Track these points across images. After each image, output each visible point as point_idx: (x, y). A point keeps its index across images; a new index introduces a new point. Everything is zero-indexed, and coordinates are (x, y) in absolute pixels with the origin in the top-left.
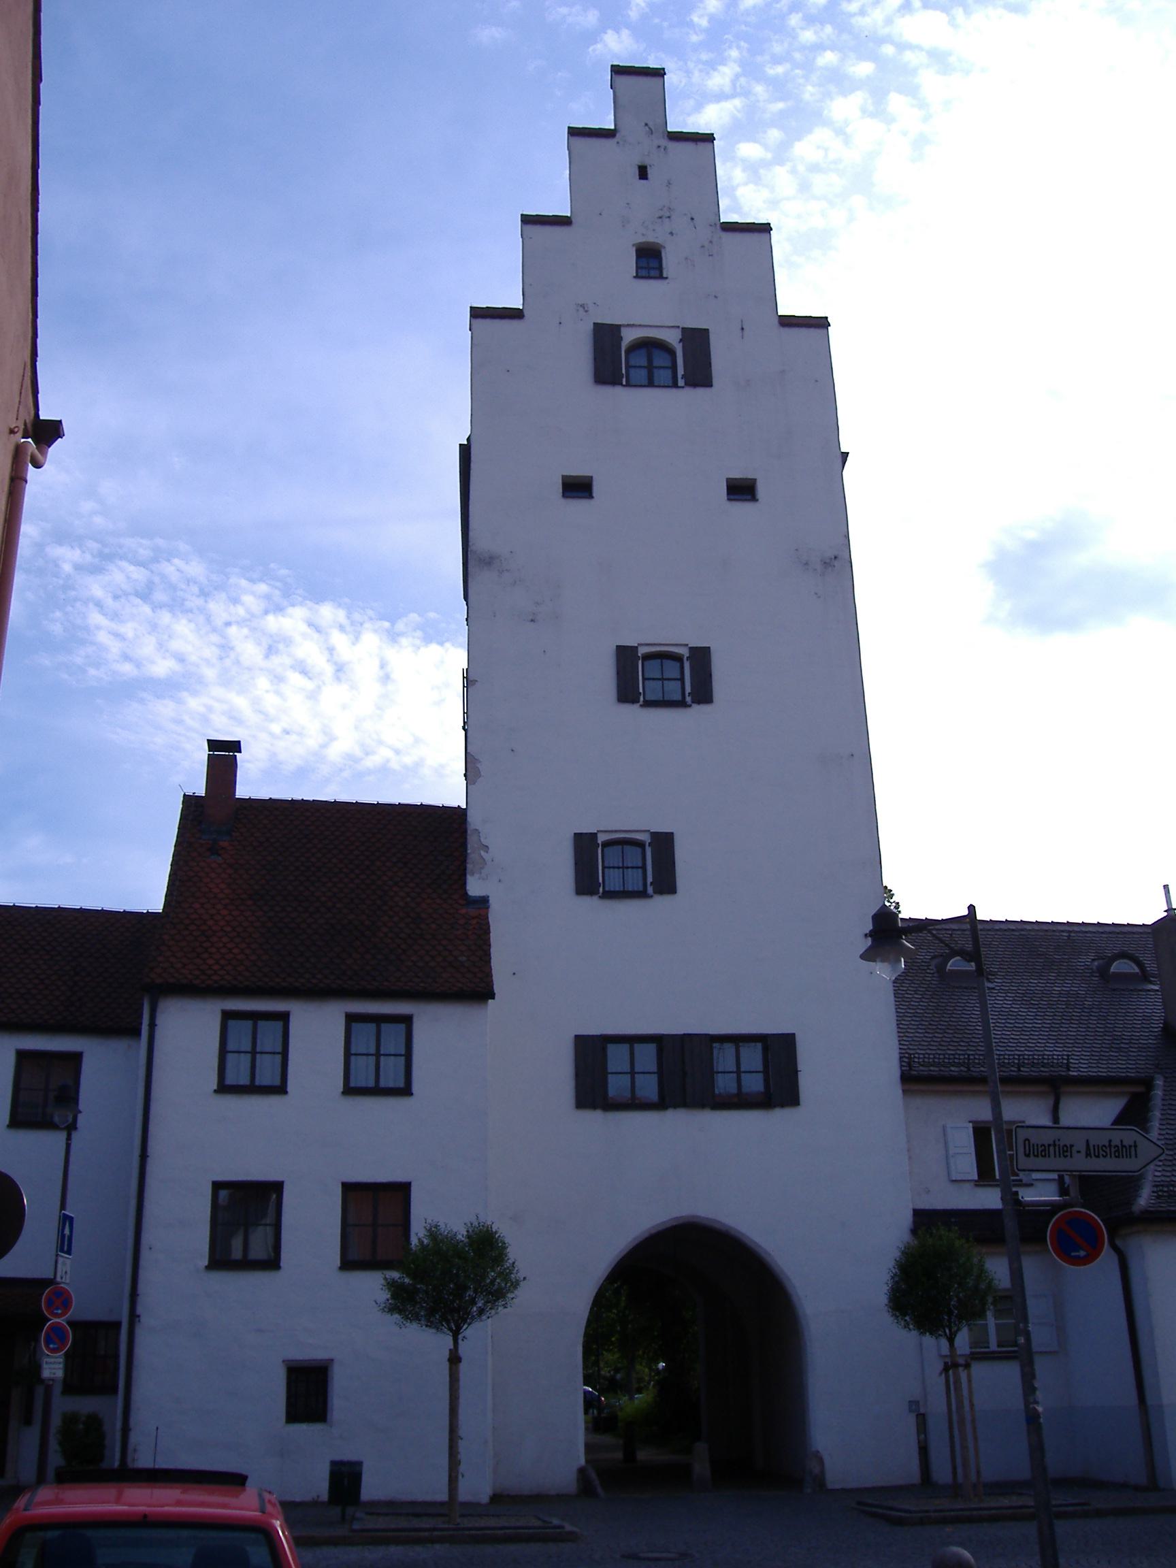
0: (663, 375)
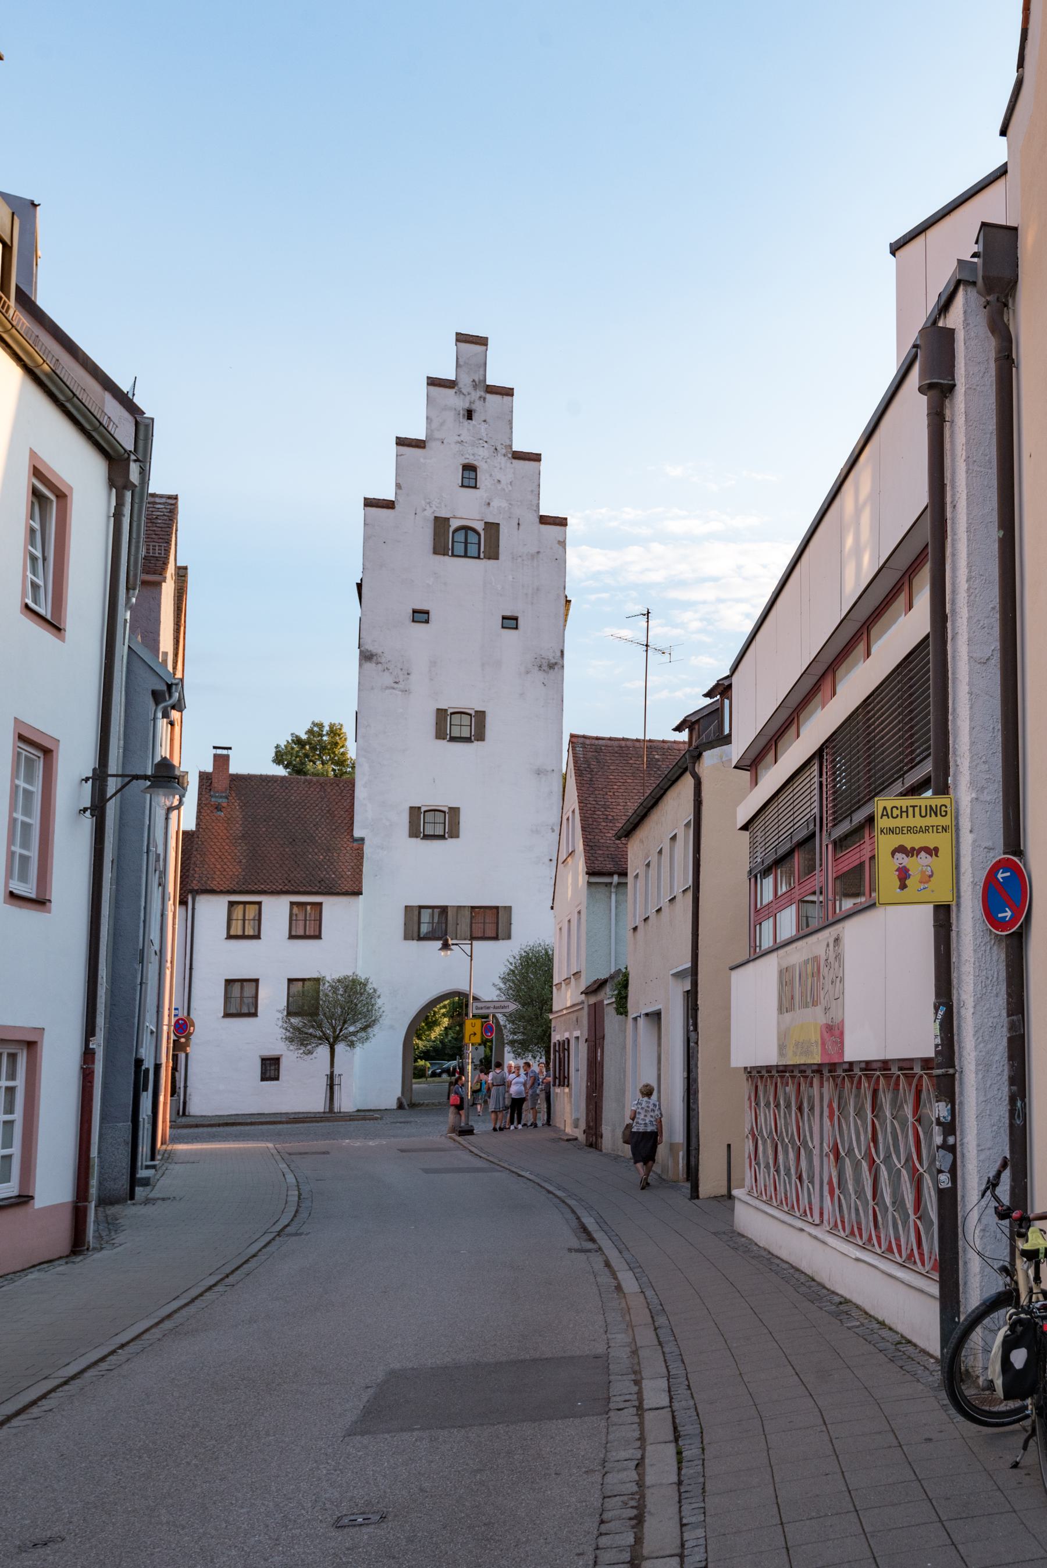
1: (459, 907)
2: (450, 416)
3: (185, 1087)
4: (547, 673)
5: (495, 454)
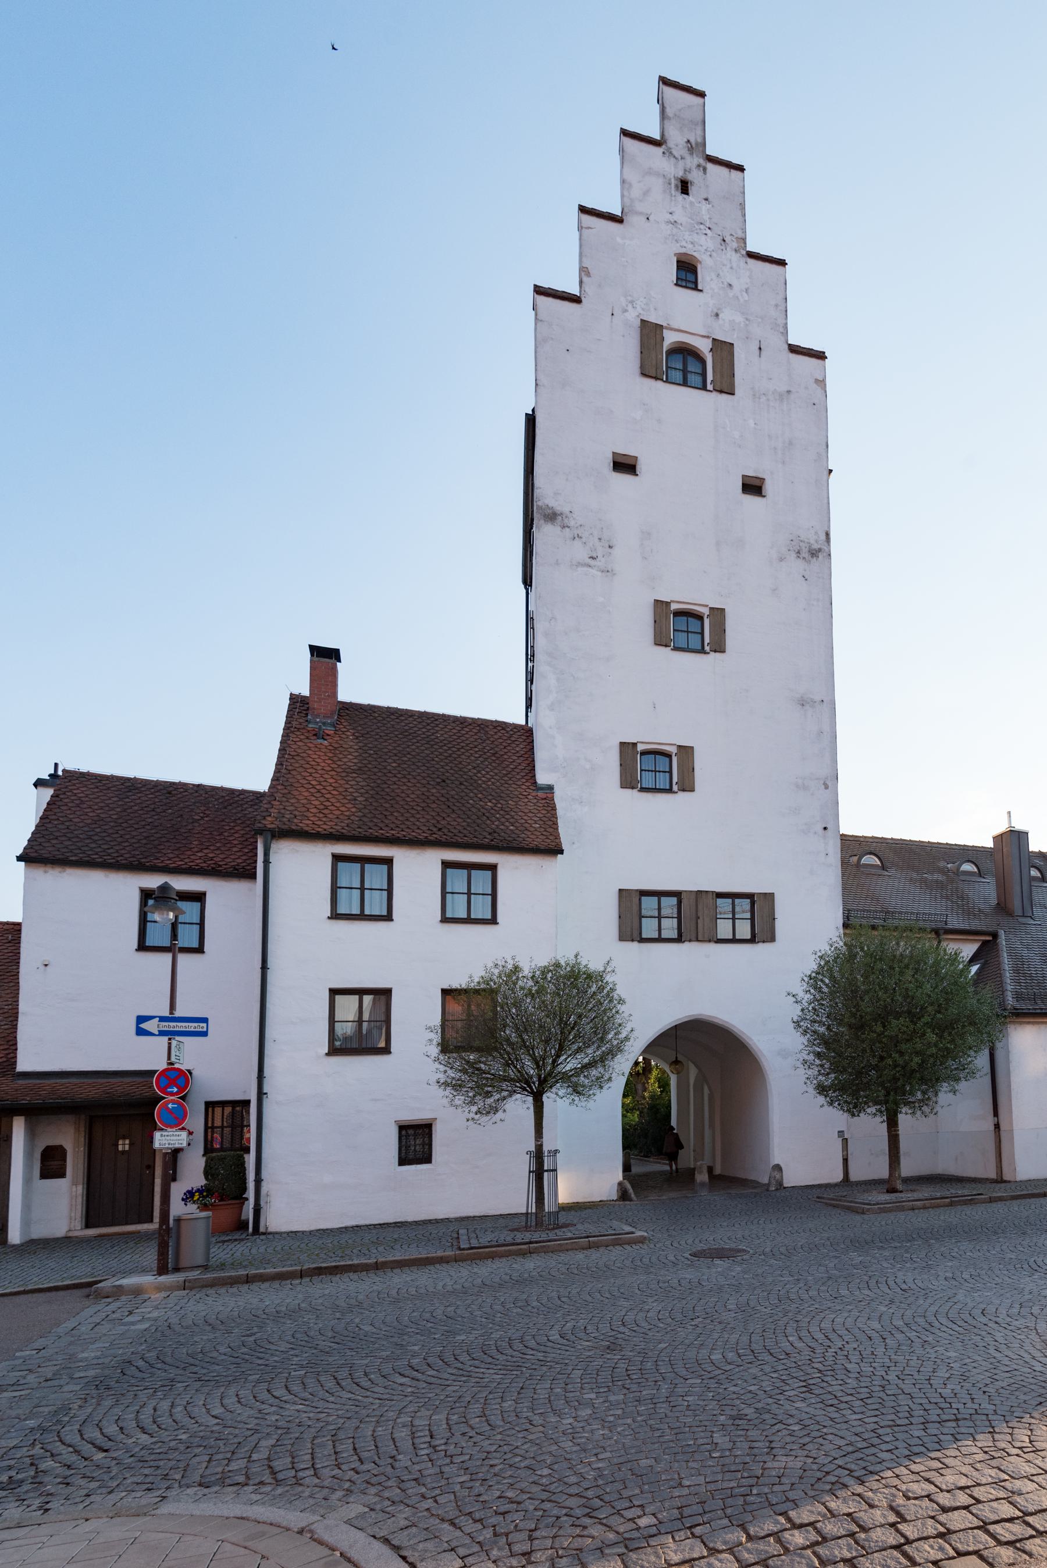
0: (694, 379)
1: (699, 893)
2: (657, 185)
3: (258, 1181)
4: (809, 562)
5: (723, 248)
